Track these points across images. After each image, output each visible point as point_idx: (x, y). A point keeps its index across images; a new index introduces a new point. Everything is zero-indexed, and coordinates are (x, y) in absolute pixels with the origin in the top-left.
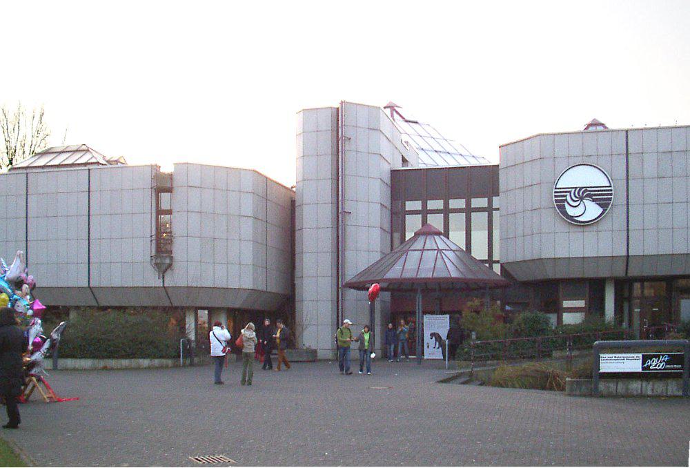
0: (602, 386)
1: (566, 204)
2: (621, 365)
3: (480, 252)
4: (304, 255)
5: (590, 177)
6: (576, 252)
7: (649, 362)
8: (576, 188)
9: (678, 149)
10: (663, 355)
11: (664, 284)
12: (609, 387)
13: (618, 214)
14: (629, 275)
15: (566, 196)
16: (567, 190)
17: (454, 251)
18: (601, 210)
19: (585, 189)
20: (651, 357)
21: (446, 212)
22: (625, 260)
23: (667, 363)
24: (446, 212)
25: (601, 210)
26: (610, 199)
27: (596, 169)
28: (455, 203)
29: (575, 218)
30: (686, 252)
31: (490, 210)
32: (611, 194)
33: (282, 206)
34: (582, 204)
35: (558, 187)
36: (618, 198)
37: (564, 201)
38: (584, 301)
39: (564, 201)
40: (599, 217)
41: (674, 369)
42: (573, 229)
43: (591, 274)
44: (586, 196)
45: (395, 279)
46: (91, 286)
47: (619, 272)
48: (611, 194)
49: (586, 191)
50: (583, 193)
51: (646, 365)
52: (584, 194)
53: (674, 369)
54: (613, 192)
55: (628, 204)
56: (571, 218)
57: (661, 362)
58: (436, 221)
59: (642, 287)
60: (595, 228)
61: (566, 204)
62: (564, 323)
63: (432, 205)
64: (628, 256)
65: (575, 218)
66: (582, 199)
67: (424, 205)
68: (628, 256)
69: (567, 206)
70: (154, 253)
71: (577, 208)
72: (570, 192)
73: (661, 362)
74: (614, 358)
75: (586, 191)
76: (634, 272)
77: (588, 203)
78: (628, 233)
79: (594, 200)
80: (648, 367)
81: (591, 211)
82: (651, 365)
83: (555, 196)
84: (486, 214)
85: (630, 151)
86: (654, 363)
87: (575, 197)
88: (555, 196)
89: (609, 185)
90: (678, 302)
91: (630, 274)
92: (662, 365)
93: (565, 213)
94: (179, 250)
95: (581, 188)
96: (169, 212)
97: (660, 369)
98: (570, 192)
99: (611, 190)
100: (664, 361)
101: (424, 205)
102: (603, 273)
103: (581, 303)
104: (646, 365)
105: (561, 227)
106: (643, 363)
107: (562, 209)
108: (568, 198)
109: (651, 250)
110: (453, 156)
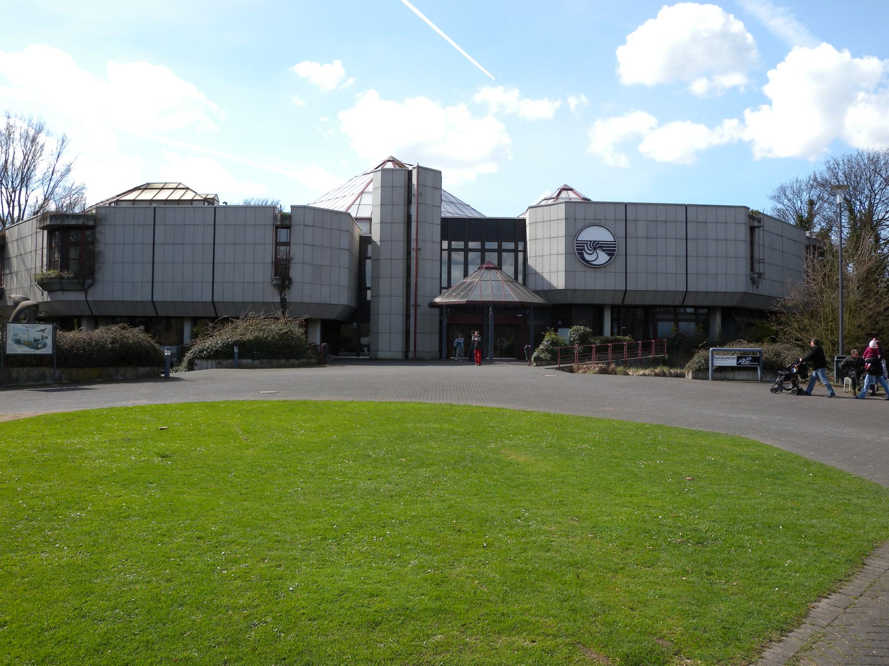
0: (15, 372)
1: (584, 253)
2: (725, 362)
4: (380, 279)
6: (590, 286)
7: (741, 361)
8: (591, 241)
9: (660, 219)
11: (438, 310)
13: (620, 261)
16: (586, 242)
18: (608, 258)
19: (598, 242)
21: (500, 251)
22: (685, 293)
23: (751, 361)
24: (500, 251)
25: (608, 258)
26: (615, 250)
27: (605, 229)
28: (490, 245)
30: (635, 289)
31: (516, 251)
32: (616, 247)
33: (745, 241)
35: (614, 240)
37: (582, 250)
39: (582, 250)
40: (607, 262)
44: (598, 247)
46: (83, 293)
47: (618, 301)
48: (616, 247)
49: (598, 244)
52: (596, 246)
54: (617, 246)
56: (587, 262)
58: (492, 258)
59: (704, 314)
60: (603, 270)
63: (472, 245)
64: (626, 290)
66: (595, 249)
68: (626, 290)
69: (584, 253)
71: (589, 256)
75: (598, 244)
76: (629, 301)
77: (600, 252)
79: (604, 251)
80: (740, 363)
83: (576, 246)
87: (591, 247)
88: (576, 246)
89: (614, 240)
91: (626, 302)
93: (583, 258)
94: (295, 273)
95: (595, 242)
96: (287, 244)
98: (587, 244)
105: (580, 267)
106: (738, 361)
107: (581, 255)
108: (584, 249)
109: (642, 287)
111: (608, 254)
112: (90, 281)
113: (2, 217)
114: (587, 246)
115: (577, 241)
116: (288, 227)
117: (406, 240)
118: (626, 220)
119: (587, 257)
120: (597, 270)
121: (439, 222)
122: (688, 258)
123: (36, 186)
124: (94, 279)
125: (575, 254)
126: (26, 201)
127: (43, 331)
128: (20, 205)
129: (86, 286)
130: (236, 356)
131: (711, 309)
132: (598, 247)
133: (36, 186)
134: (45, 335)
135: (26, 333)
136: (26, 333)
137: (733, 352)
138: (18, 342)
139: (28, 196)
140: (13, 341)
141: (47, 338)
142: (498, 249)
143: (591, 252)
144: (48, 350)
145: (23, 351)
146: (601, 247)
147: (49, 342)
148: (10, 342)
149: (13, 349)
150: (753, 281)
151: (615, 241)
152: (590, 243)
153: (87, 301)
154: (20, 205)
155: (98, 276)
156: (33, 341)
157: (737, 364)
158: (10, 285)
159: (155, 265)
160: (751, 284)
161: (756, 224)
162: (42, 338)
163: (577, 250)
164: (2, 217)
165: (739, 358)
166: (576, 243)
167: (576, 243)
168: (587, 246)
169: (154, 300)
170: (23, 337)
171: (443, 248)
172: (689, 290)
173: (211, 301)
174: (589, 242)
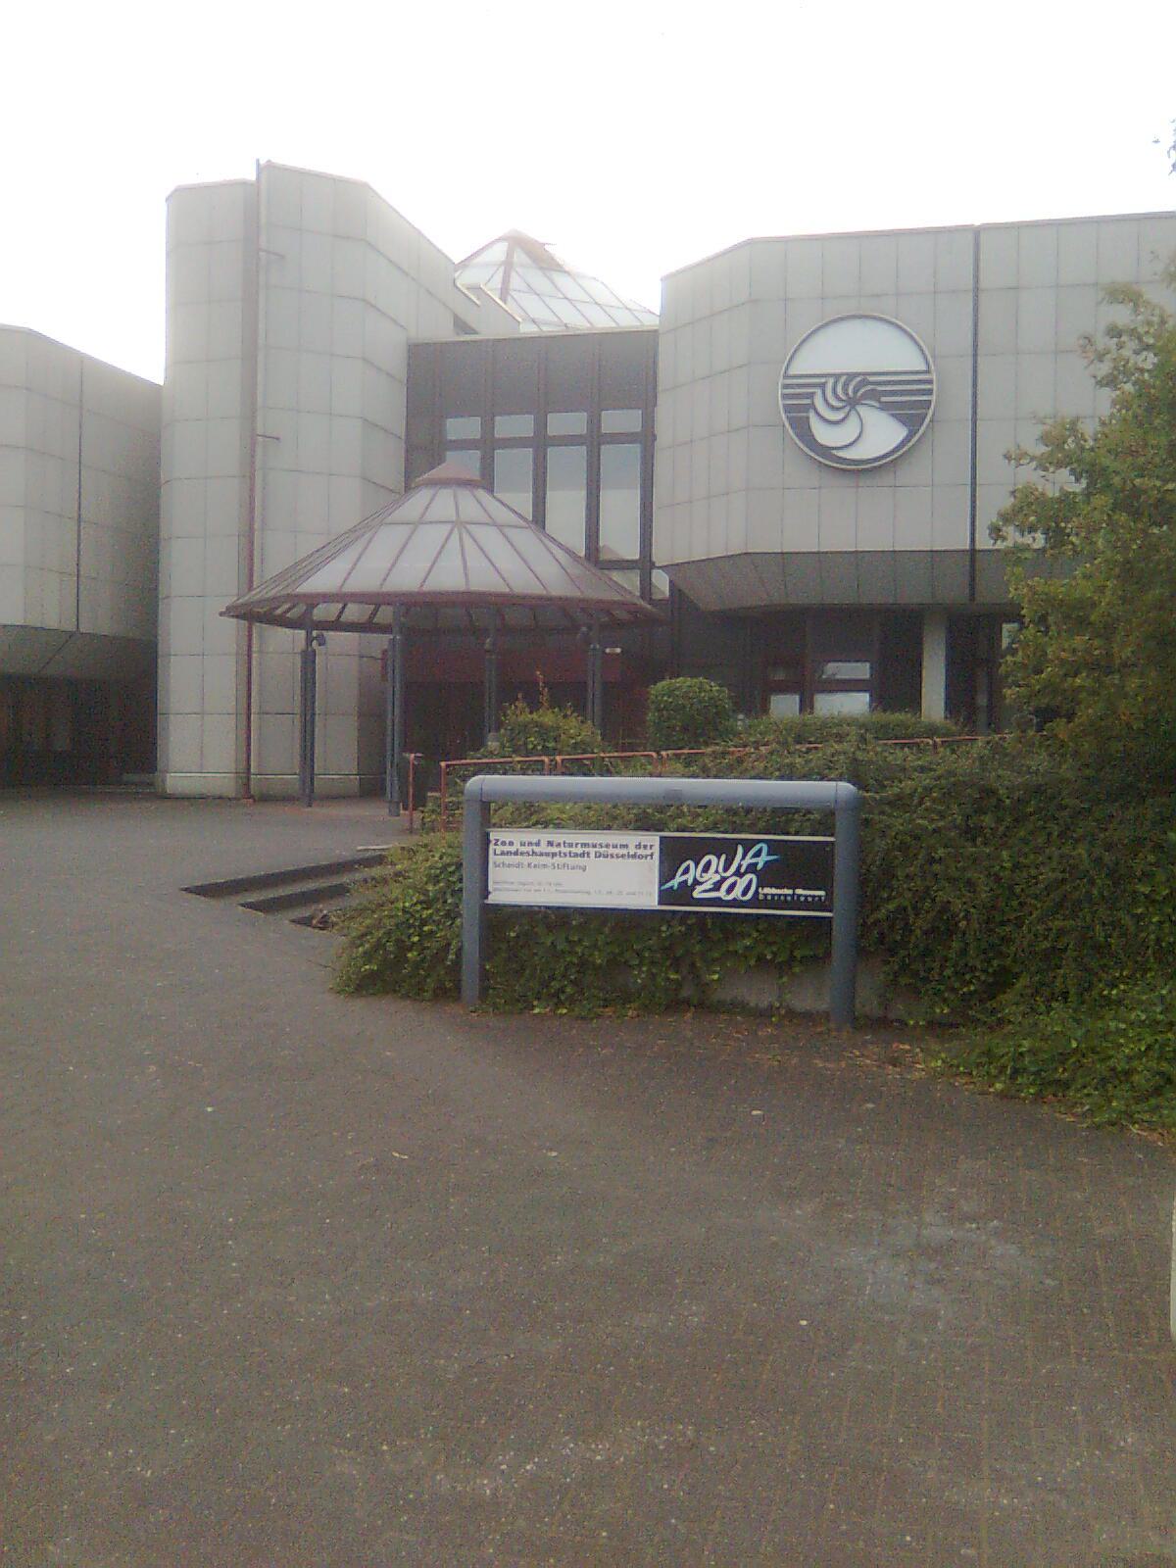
3: (622, 540)
8: (837, 376)
10: (748, 845)
14: (979, 599)
15: (811, 396)
16: (819, 382)
17: (500, 527)
20: (695, 850)
27: (885, 327)
29: (835, 452)
34: (853, 419)
35: (792, 372)
36: (952, 402)
37: (807, 408)
38: (868, 665)
41: (806, 905)
44: (865, 396)
45: (458, 593)
47: (953, 591)
48: (930, 392)
50: (855, 391)
51: (675, 883)
53: (806, 905)
56: (826, 451)
57: (738, 873)
61: (812, 415)
65: (835, 452)
66: (852, 403)
67: (488, 426)
71: (867, 430)
73: (738, 873)
74: (544, 848)
79: (885, 407)
80: (686, 889)
81: (880, 433)
82: (696, 882)
84: (636, 449)
85: (983, 285)
86: (712, 877)
89: (924, 368)
90: (634, 568)
92: (742, 883)
95: (851, 376)
97: (735, 903)
98: (823, 386)
99: (930, 382)
100: (752, 868)
101: (488, 426)
102: (913, 592)
103: (862, 670)
104: (675, 883)
106: (666, 875)
108: (813, 406)
110: (547, 300)
111: (903, 420)
113: (863, 402)
114: (824, 393)
118: (976, 290)
119: (824, 435)
132: (865, 396)
137: (644, 817)
142: (545, 435)
143: (839, 416)
146: (874, 395)
151: (928, 372)
157: (665, 896)
158: (506, 882)
164: (863, 402)
165: (674, 855)
166: (786, 386)
167: (786, 386)
168: (824, 393)
172: (978, 546)
174: (831, 381)
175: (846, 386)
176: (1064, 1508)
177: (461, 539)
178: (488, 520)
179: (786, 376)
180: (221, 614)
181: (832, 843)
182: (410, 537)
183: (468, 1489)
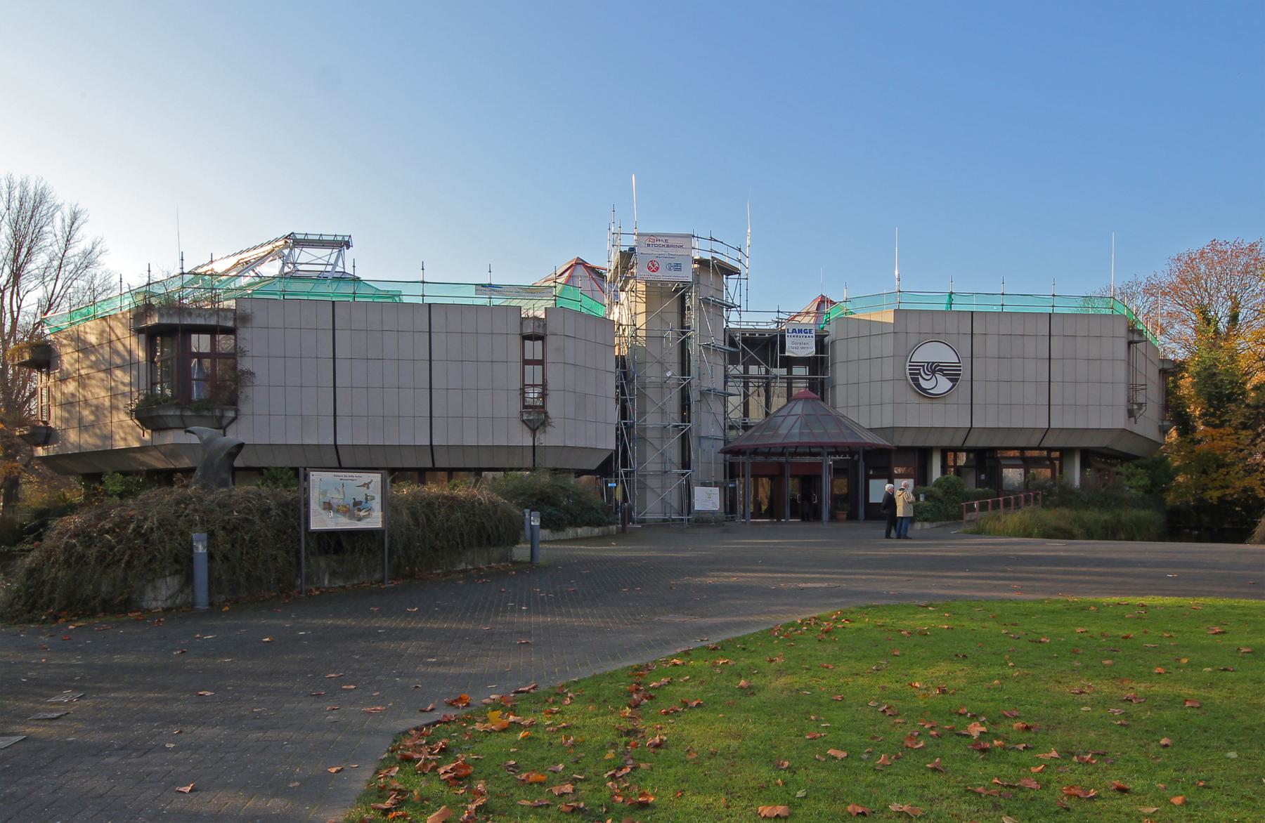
1: (920, 378)
5: (944, 355)
8: (929, 363)
12: (577, 532)
13: (964, 385)
18: (951, 384)
25: (951, 384)
27: (942, 344)
32: (960, 370)
35: (912, 361)
36: (965, 374)
42: (922, 400)
43: (920, 443)
44: (938, 371)
48: (960, 370)
55: (430, 332)
56: (924, 390)
62: (887, 521)
63: (753, 370)
64: (534, 446)
66: (934, 373)
70: (298, 237)
72: (923, 366)
75: (939, 366)
78: (1049, 407)
81: (943, 384)
83: (910, 369)
88: (910, 369)
89: (912, 361)
93: (919, 386)
95: (933, 363)
98: (923, 366)
99: (960, 366)
105: (912, 397)
107: (916, 380)
108: (920, 374)
111: (951, 380)
112: (231, 414)
115: (910, 362)
116: (541, 338)
117: (680, 361)
119: (924, 384)
120: (934, 401)
121: (612, 366)
122: (1051, 383)
123: (31, 286)
124: (237, 411)
125: (907, 380)
126: (19, 308)
127: (367, 485)
128: (12, 312)
129: (225, 422)
130: (977, 510)
131: (1066, 452)
132: (938, 371)
133: (31, 286)
134: (369, 493)
135: (341, 490)
136: (341, 490)
138: (328, 506)
139: (21, 300)
140: (320, 506)
141: (373, 498)
144: (374, 520)
145: (1043, 544)
146: (941, 370)
147: (376, 505)
148: (314, 506)
149: (321, 521)
150: (1131, 414)
151: (960, 363)
152: (928, 366)
153: (336, 445)
154: (12, 312)
155: (244, 408)
156: (352, 505)
159: (338, 390)
160: (1127, 417)
161: (1136, 338)
162: (366, 499)
163: (911, 374)
166: (910, 366)
167: (910, 366)
169: (338, 443)
170: (336, 497)
171: (526, 383)
173: (429, 444)
174: (926, 364)
175: (931, 366)
176: (376, 679)
177: (798, 419)
178: (791, 413)
179: (910, 362)
180: (719, 453)
181: (752, 519)
182: (1042, 440)
183: (424, 742)
